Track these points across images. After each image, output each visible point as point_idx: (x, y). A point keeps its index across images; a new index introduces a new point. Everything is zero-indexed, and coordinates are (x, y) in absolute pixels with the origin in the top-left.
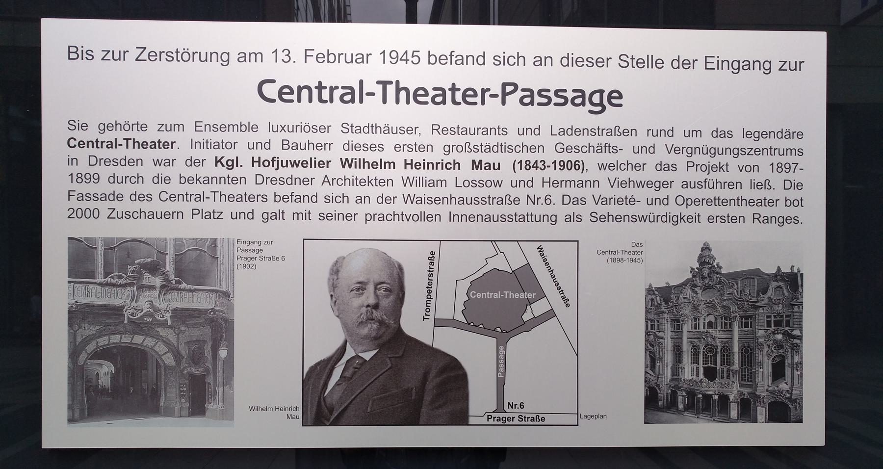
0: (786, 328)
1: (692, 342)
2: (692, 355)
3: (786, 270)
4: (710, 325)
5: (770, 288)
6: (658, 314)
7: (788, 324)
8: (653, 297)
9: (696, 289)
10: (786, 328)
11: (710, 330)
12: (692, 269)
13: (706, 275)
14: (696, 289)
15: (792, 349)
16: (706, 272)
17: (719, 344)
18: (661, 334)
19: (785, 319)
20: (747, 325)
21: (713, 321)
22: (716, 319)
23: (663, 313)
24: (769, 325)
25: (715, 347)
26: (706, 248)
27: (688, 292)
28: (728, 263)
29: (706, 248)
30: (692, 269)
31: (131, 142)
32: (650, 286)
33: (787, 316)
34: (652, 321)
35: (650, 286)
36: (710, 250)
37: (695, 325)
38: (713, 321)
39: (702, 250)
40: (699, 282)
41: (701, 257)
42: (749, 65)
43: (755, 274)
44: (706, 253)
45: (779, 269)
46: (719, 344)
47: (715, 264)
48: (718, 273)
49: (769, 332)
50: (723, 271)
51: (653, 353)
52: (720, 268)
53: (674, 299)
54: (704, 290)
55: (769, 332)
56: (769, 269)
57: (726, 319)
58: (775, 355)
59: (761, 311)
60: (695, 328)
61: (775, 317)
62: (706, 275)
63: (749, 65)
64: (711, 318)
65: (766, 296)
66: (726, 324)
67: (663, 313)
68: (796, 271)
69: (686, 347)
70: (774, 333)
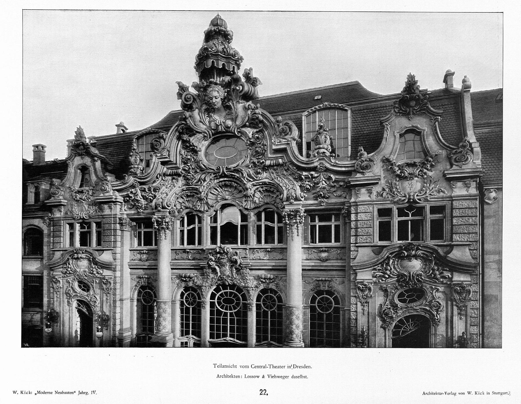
0: (431, 243)
1: (180, 277)
2: (184, 311)
3: (430, 83)
4: (229, 233)
5: (388, 135)
6: (99, 204)
7: (437, 231)
8: (87, 161)
9: (193, 140)
10: (431, 243)
11: (229, 247)
12: (182, 89)
13: (218, 102)
14: (193, 140)
15: (449, 299)
16: (217, 94)
17: (252, 283)
18: (106, 257)
19: (429, 217)
20: (325, 236)
21: (237, 221)
22: (244, 218)
23: (110, 202)
24: (385, 232)
25: (241, 292)
26: (217, 33)
27: (172, 147)
28: (275, 69)
29: (217, 33)
30: (182, 89)
31: (271, 366)
32: (79, 134)
33: (434, 210)
34: (84, 223)
35: (79, 134)
36: (226, 37)
37: (191, 233)
38: (237, 221)
39: (209, 36)
40: (197, 117)
41: (202, 58)
42: (504, 393)
43: (349, 96)
44: (217, 45)
45: (411, 84)
46: (252, 283)
47: (240, 73)
48: (247, 97)
49: (385, 253)
50: (263, 92)
51: (87, 305)
52: (252, 81)
53: (138, 167)
54: (215, 141)
55: (385, 253)
56: (386, 85)
57: (270, 217)
58: (401, 314)
59: (363, 195)
60: (191, 242)
61: (401, 212)
62: (218, 102)
63: (504, 393)
64: (233, 215)
65: (377, 157)
66: (269, 231)
67: (110, 202)
68: (457, 86)
69: (168, 290)
70: (399, 256)
